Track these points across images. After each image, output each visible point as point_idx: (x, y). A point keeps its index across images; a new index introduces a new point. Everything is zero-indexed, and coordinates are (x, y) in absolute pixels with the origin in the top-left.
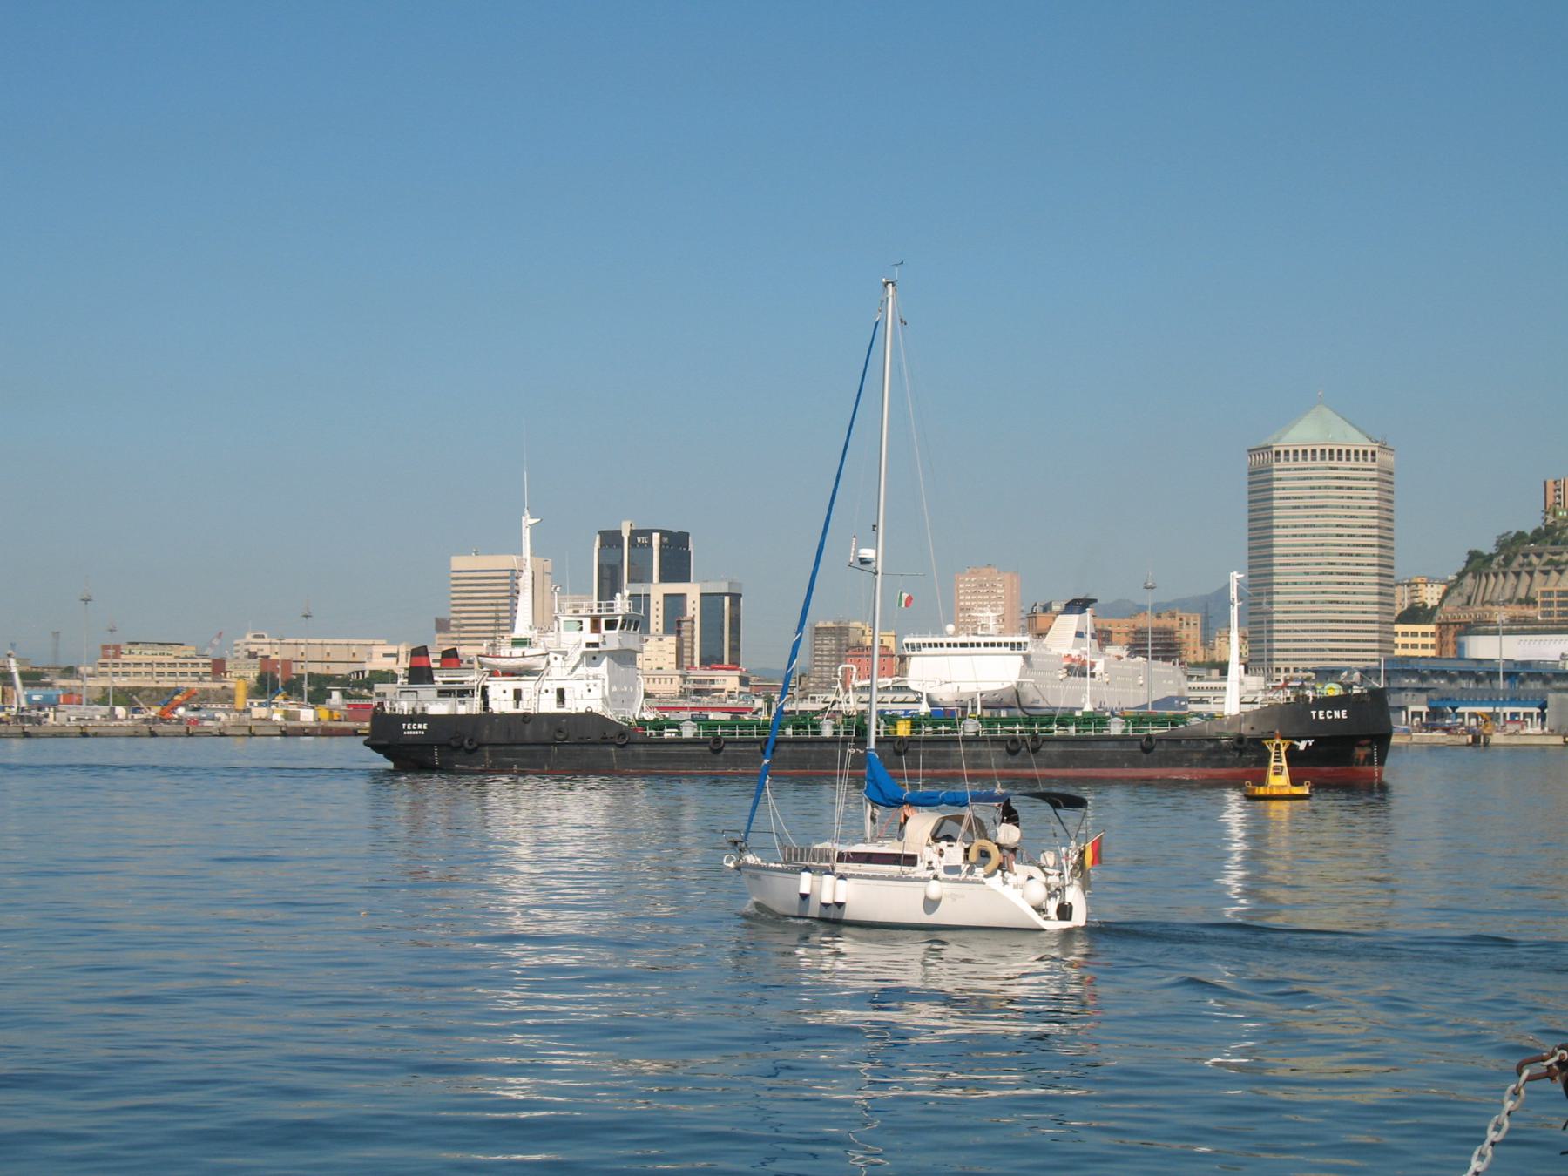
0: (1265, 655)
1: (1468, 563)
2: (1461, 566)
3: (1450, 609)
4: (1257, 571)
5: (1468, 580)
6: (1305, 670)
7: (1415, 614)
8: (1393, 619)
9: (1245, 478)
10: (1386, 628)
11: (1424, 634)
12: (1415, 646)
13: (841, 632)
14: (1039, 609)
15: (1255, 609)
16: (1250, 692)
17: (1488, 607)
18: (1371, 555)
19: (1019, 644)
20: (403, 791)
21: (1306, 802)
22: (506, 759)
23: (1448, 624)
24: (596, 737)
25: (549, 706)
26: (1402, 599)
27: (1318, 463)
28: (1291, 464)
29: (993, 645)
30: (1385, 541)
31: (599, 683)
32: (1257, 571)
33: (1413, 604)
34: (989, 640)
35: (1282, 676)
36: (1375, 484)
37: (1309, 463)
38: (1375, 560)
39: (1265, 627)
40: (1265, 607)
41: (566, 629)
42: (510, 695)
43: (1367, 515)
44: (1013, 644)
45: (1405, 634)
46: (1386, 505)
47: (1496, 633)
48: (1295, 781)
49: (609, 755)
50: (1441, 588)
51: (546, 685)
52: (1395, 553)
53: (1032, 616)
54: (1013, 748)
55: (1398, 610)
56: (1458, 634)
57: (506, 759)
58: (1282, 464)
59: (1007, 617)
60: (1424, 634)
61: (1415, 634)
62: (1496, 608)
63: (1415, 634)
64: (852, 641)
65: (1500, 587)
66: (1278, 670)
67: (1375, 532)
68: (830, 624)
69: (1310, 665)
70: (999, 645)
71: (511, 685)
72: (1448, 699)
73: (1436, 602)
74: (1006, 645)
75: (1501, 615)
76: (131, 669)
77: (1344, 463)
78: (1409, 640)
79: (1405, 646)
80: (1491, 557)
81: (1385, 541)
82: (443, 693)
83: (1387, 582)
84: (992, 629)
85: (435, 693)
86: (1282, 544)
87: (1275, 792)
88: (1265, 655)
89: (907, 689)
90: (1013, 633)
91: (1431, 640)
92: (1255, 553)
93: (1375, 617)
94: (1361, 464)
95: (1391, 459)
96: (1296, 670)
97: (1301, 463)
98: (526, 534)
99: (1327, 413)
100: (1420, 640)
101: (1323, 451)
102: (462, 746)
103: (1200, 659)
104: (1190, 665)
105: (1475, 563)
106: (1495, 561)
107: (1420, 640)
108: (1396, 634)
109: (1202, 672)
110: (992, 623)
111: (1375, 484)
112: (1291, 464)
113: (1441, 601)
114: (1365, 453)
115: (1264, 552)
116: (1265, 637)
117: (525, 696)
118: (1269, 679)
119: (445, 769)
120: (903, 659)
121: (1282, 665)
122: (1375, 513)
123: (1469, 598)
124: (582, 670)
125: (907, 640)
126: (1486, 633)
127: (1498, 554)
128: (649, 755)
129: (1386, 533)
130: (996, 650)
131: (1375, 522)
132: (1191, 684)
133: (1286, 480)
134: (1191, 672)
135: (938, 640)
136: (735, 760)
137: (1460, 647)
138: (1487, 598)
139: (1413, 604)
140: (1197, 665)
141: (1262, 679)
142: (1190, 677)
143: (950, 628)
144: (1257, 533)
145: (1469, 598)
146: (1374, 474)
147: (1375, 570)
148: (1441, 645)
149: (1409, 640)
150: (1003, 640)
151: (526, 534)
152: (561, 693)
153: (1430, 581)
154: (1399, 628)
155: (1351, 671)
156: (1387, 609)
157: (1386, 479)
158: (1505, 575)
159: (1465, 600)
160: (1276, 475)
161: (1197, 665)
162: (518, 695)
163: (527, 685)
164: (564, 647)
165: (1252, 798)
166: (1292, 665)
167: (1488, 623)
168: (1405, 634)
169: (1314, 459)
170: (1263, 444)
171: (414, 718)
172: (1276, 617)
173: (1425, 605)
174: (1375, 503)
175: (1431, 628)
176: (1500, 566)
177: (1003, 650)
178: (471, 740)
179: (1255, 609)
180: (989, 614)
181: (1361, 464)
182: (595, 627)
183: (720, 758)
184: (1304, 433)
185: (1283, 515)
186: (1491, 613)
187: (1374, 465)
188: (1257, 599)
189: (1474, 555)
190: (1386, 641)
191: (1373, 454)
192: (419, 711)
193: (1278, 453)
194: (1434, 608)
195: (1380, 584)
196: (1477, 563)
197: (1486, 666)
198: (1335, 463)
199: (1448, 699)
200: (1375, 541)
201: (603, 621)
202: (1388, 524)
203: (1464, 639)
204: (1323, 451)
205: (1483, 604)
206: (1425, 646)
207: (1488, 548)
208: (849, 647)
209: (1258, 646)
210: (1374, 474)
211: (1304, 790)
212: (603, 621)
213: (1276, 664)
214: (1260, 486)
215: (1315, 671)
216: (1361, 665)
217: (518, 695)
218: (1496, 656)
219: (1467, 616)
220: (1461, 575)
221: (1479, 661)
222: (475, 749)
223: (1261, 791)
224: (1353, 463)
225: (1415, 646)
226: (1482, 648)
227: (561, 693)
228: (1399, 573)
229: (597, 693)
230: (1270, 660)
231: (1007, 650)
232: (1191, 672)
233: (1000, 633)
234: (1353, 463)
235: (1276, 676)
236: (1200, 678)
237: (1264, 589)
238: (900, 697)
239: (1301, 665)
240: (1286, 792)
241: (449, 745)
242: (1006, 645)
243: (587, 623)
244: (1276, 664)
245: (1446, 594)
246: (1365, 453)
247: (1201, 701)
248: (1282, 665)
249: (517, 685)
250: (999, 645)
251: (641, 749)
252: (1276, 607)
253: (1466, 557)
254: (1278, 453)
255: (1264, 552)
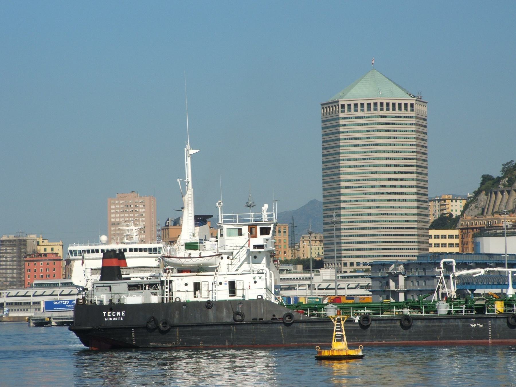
0: (335, 254)
1: (482, 184)
2: (477, 186)
3: (469, 218)
4: (329, 193)
5: (483, 197)
6: (365, 264)
7: (444, 222)
8: (428, 225)
9: (320, 125)
10: (423, 232)
11: (451, 237)
12: (444, 245)
13: (21, 243)
14: (171, 223)
15: (327, 220)
16: (325, 281)
17: (497, 216)
18: (411, 180)
19: (155, 249)
20: (104, 363)
21: (360, 361)
22: (194, 338)
23: (468, 229)
24: (268, 317)
25: (222, 295)
26: (434, 211)
27: (372, 113)
28: (353, 114)
29: (136, 250)
30: (422, 169)
31: (263, 276)
32: (329, 193)
33: (442, 215)
34: (133, 246)
35: (348, 268)
36: (414, 128)
37: (366, 113)
38: (414, 183)
39: (335, 233)
40: (334, 219)
41: (229, 235)
42: (191, 287)
43: (408, 151)
44: (150, 249)
45: (437, 237)
46: (422, 143)
47: (502, 235)
48: (350, 347)
49: (278, 332)
50: (464, 202)
51: (219, 279)
52: (429, 178)
53: (166, 228)
54: (406, 323)
55: (432, 219)
56: (475, 236)
57: (194, 338)
58: (346, 114)
59: (147, 229)
60: (451, 237)
61: (444, 237)
62: (503, 216)
63: (444, 237)
64: (30, 250)
65: (501, 200)
66: (345, 264)
67: (414, 162)
68: (12, 237)
69: (368, 260)
70: (141, 250)
71: (191, 279)
72: (468, 284)
73: (459, 213)
74: (145, 250)
75: (506, 221)
76: (361, 267)
77: (391, 113)
78: (440, 241)
79: (437, 245)
80: (499, 179)
81: (422, 169)
82: (134, 287)
83: (423, 199)
84: (136, 238)
85: (126, 287)
86: (347, 173)
87: (336, 354)
88: (335, 254)
89: (71, 285)
90: (151, 241)
91: (456, 241)
92: (328, 179)
93: (415, 225)
94: (403, 113)
95: (425, 109)
96: (358, 264)
97: (360, 113)
98: (188, 162)
99: (378, 76)
100: (447, 241)
101: (369, 104)
102: (158, 327)
103: (289, 258)
104: (281, 262)
105: (487, 184)
106: (502, 182)
107: (447, 241)
108: (430, 237)
109: (291, 267)
110: (135, 233)
111: (414, 128)
112: (353, 114)
113: (463, 212)
114: (406, 105)
115: (334, 171)
116: (335, 240)
117: (203, 287)
118: (339, 271)
119: (141, 347)
120: (69, 262)
121: (348, 261)
122: (414, 148)
123: (483, 210)
124: (246, 267)
125: (71, 248)
126: (495, 235)
127: (503, 178)
128: (310, 331)
129: (421, 163)
130: (138, 254)
131: (414, 155)
132: (282, 276)
133: (349, 126)
134: (282, 267)
135: (94, 247)
136: (380, 334)
137: (477, 245)
138: (496, 209)
139: (442, 215)
140: (286, 262)
141: (333, 271)
142: (282, 271)
143: (104, 238)
144: (328, 165)
145: (483, 210)
146: (413, 121)
147: (414, 190)
148: (463, 244)
149: (440, 241)
150: (143, 246)
151: (188, 162)
152: (232, 285)
153: (455, 198)
154: (432, 232)
155: (397, 264)
156: (423, 218)
157: (422, 123)
158: (509, 192)
159: (480, 211)
160: (342, 122)
161: (286, 262)
162: (197, 286)
163: (206, 280)
164: (228, 249)
165: (320, 358)
166: (355, 261)
167: (497, 228)
168: (437, 237)
169: (363, 110)
170: (332, 99)
171: (112, 307)
172: (343, 226)
173: (451, 215)
174: (414, 142)
175: (456, 232)
176: (505, 185)
177: (143, 254)
178: (165, 323)
179: (327, 220)
180: (133, 227)
181: (403, 113)
182: (252, 234)
183: (368, 332)
184: (362, 91)
185: (347, 151)
186: (499, 220)
187: (413, 114)
188: (328, 213)
189: (486, 178)
190: (423, 242)
191: (412, 105)
192: (116, 302)
193: (343, 106)
194: (458, 217)
195: (418, 201)
196: (489, 184)
197: (496, 259)
198: (384, 113)
199: (468, 284)
200: (414, 169)
201: (258, 228)
202: (423, 157)
203: (479, 239)
204: (375, 104)
205: (493, 214)
206: (451, 245)
207: (496, 173)
208: (27, 254)
209: (330, 247)
210: (413, 121)
211: (359, 352)
212: (258, 228)
213: (344, 260)
214: (331, 129)
215: (371, 265)
216: (404, 260)
217: (197, 286)
218: (502, 252)
219: (482, 223)
220: (477, 193)
221: (490, 255)
222: (168, 330)
223: (326, 353)
224: (397, 113)
225: (444, 245)
226: (492, 245)
227: (232, 285)
228: (432, 193)
229: (261, 284)
230: (340, 257)
231: (146, 254)
232: (282, 267)
233: (142, 241)
234: (397, 113)
235: (344, 269)
236: (289, 271)
237: (334, 206)
238: (67, 291)
239: (362, 260)
240: (344, 353)
241: (146, 328)
242: (145, 250)
243: (245, 230)
244: (344, 260)
245: (466, 207)
246: (406, 105)
247: (289, 288)
248: (348, 261)
249: (197, 279)
250: (141, 250)
251: (303, 326)
252: (343, 219)
253: (480, 180)
254: (343, 106)
255: (334, 178)
